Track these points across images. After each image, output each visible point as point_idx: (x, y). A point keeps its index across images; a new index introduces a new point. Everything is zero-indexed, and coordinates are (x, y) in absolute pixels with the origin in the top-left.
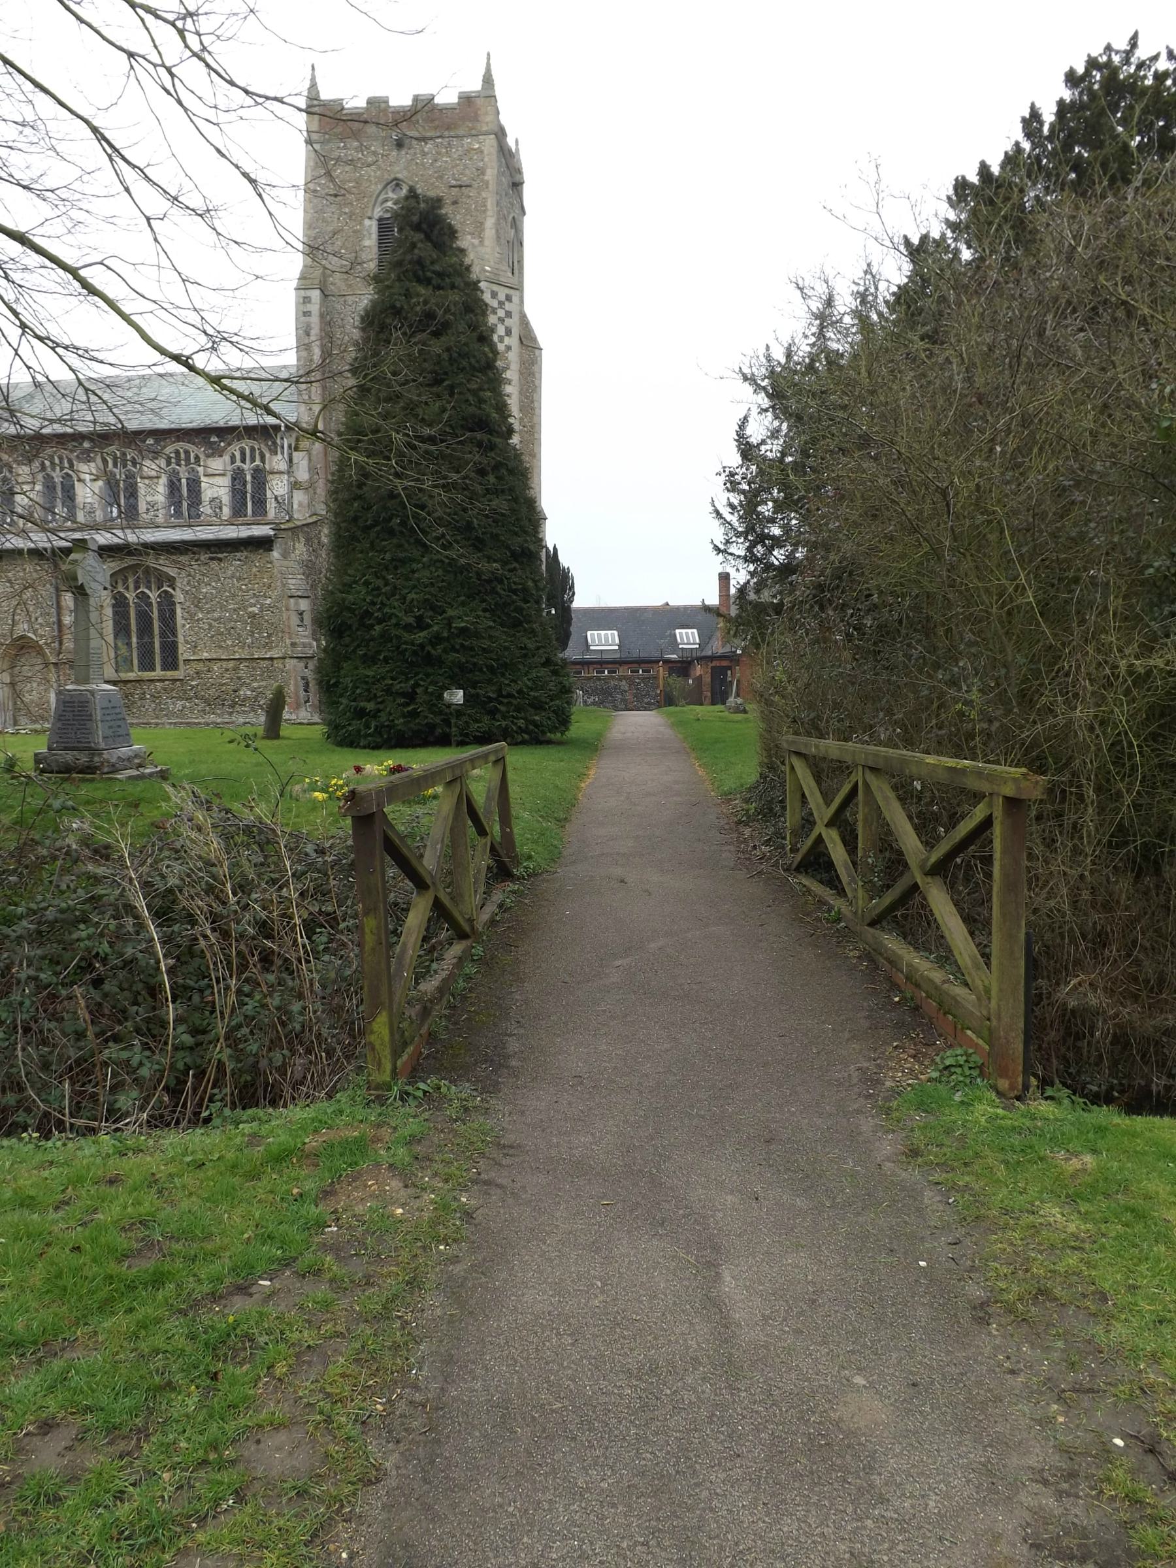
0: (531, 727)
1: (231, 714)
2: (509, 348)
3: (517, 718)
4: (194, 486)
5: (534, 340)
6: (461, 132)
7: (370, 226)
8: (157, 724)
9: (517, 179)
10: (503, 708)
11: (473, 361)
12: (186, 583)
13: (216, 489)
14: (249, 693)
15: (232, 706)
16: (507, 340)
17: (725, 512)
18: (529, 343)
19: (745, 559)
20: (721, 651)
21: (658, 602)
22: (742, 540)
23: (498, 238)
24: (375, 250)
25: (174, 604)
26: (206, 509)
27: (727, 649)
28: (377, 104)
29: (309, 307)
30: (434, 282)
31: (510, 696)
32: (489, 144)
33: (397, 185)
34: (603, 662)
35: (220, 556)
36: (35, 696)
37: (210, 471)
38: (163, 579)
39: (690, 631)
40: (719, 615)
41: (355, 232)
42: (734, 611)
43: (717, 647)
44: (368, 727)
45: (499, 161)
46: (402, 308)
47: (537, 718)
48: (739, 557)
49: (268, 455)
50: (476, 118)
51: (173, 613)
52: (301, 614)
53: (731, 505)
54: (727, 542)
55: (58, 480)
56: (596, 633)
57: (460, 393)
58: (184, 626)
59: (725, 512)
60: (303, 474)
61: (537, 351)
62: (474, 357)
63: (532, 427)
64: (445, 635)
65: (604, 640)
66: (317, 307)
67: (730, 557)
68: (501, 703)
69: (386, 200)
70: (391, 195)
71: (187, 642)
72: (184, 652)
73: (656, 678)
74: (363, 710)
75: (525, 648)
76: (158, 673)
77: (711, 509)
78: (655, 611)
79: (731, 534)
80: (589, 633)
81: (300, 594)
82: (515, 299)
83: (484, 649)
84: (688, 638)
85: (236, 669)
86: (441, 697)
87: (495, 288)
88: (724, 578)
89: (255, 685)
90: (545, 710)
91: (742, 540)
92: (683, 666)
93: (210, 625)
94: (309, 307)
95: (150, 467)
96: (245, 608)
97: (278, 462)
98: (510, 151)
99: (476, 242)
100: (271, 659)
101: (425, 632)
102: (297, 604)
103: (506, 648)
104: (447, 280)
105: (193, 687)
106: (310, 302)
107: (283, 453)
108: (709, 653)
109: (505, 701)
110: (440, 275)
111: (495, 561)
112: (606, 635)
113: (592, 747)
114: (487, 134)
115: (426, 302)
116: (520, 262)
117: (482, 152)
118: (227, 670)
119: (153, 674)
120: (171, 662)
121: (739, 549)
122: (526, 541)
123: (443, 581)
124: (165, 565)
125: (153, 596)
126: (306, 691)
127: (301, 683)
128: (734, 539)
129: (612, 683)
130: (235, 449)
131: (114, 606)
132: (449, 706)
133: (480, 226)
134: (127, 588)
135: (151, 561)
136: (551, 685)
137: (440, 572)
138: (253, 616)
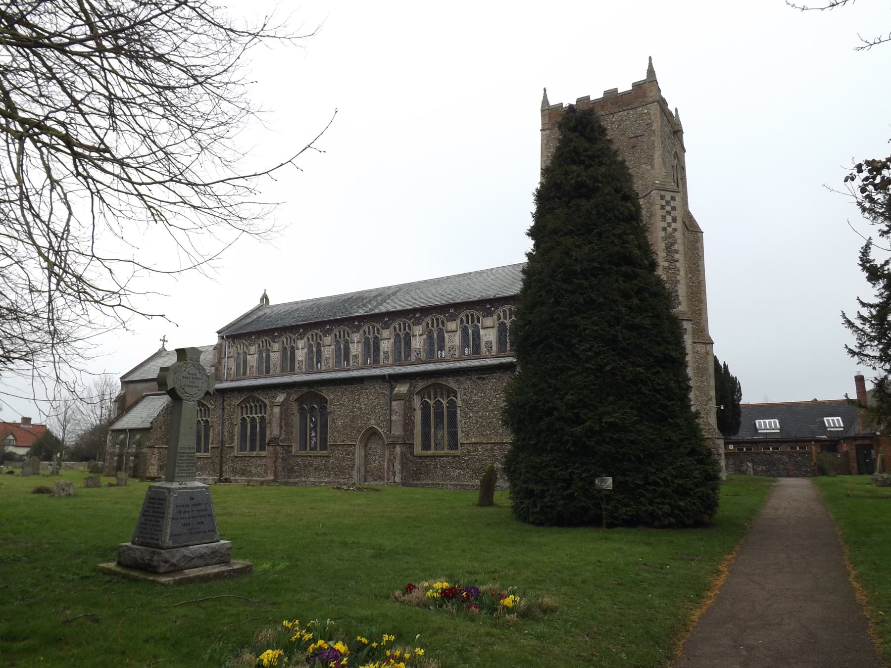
0: (677, 512)
2: (675, 230)
3: (663, 503)
4: (477, 336)
5: (697, 226)
6: (635, 106)
8: (443, 485)
9: (676, 128)
10: (649, 495)
11: (617, 213)
16: (673, 225)
17: (858, 323)
18: (693, 231)
19: (881, 359)
20: (862, 433)
21: (809, 399)
22: (876, 343)
23: (664, 163)
26: (483, 349)
27: (868, 431)
30: (587, 163)
31: (656, 484)
32: (655, 108)
34: (768, 441)
38: (452, 392)
39: (835, 418)
40: (861, 406)
42: (872, 402)
43: (858, 429)
44: (535, 506)
45: (661, 117)
46: (562, 183)
47: (682, 503)
48: (874, 357)
50: (644, 95)
53: (861, 317)
54: (862, 346)
55: (402, 336)
56: (762, 421)
57: (607, 237)
59: (858, 323)
61: (699, 234)
62: (618, 210)
63: (699, 283)
64: (597, 428)
65: (769, 425)
67: (865, 358)
68: (646, 490)
73: (810, 453)
74: (532, 491)
75: (670, 440)
77: (843, 320)
78: (806, 404)
79: (865, 339)
80: (757, 422)
82: (678, 198)
83: (632, 441)
84: (834, 423)
86: (592, 483)
87: (663, 193)
88: (860, 380)
90: (690, 496)
91: (876, 343)
92: (832, 443)
93: (477, 421)
95: (452, 325)
98: (671, 113)
99: (649, 167)
101: (581, 427)
103: (652, 441)
104: (597, 160)
108: (853, 434)
109: (651, 488)
110: (591, 158)
111: (639, 366)
112: (770, 423)
113: (738, 530)
114: (652, 102)
115: (578, 176)
116: (684, 178)
120: (453, 445)
121: (873, 350)
122: (668, 349)
123: (594, 385)
124: (452, 383)
125: (444, 402)
128: (868, 343)
129: (776, 457)
130: (500, 311)
131: (422, 409)
132: (600, 491)
133: (650, 159)
134: (430, 399)
135: (442, 381)
136: (696, 473)
137: (592, 377)
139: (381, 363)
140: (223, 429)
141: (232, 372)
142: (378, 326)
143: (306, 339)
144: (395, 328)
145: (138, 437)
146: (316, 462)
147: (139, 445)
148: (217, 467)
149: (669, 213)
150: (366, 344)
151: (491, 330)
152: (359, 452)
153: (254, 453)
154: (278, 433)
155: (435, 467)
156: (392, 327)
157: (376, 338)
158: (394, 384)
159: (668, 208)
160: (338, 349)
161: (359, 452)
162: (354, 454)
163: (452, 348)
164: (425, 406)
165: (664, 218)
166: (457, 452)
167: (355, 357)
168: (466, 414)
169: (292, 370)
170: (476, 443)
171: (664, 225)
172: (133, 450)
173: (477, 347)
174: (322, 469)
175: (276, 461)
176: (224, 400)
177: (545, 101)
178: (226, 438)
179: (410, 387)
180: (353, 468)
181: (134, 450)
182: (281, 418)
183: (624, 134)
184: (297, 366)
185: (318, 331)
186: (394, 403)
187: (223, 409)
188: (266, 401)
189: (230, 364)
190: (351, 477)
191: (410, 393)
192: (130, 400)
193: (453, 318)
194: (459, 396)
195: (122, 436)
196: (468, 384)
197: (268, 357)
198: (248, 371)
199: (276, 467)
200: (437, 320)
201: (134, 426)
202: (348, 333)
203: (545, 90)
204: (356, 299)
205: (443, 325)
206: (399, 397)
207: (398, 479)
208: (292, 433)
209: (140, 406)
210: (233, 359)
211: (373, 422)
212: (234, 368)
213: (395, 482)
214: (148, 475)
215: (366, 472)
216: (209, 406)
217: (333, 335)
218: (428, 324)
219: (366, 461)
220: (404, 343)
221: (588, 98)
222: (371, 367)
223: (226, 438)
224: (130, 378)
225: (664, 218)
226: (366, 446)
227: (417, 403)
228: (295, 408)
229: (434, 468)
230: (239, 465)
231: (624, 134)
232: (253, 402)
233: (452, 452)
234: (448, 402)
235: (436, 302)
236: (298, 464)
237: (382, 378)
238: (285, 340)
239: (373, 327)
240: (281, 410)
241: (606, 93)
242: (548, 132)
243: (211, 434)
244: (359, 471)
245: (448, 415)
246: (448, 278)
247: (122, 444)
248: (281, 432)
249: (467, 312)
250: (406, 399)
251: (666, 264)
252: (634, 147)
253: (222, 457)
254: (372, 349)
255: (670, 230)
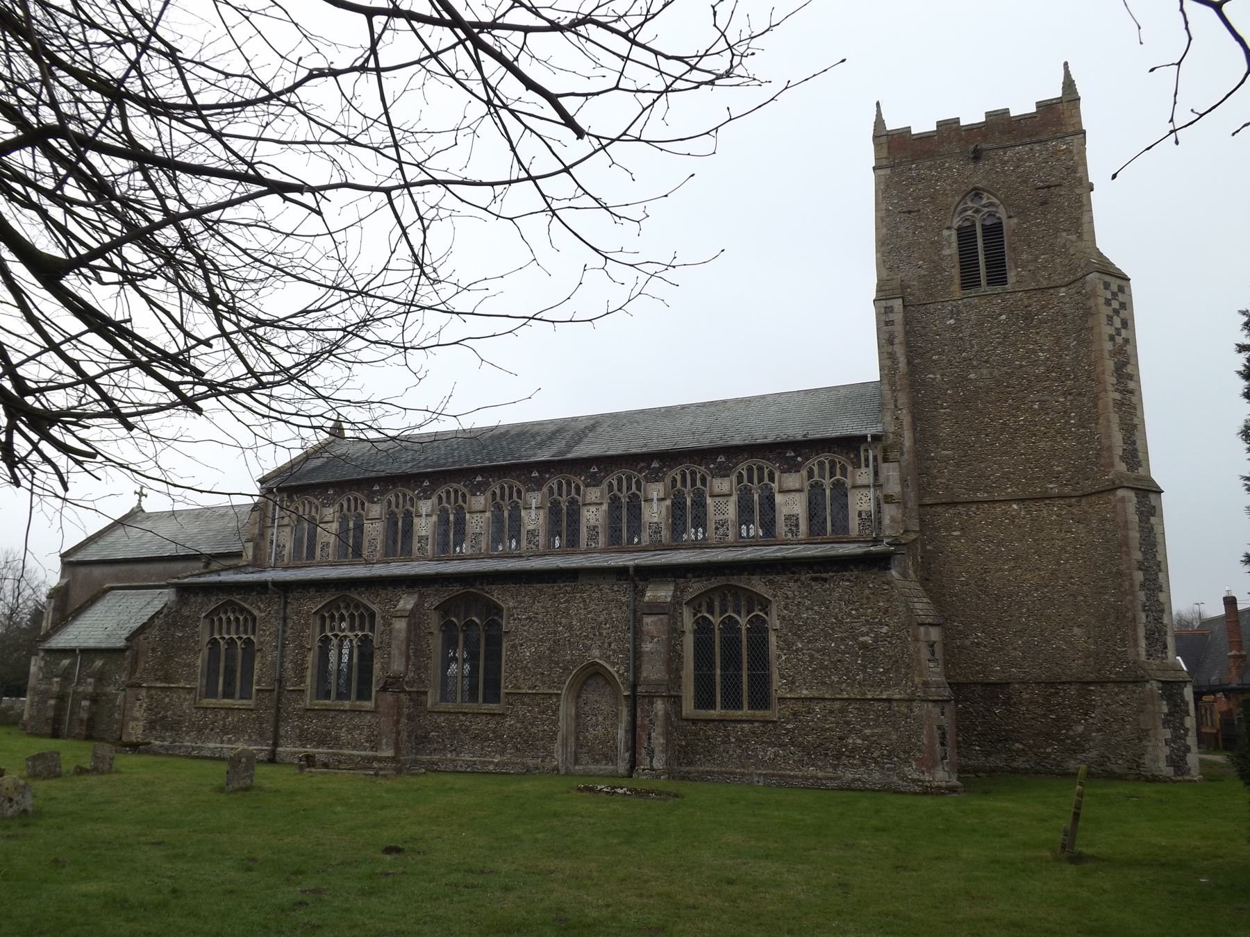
1: (835, 767)
7: (950, 236)
12: (783, 607)
13: (791, 505)
14: (859, 741)
15: (838, 757)
24: (956, 258)
25: (766, 630)
26: (781, 528)
28: (949, 128)
29: (891, 317)
33: (977, 194)
35: (824, 575)
36: (600, 731)
37: (785, 487)
41: (932, 243)
49: (709, 479)
51: (765, 642)
52: (932, 646)
58: (779, 657)
60: (894, 488)
66: (901, 315)
69: (965, 210)
70: (970, 204)
71: (782, 677)
72: (778, 685)
76: (745, 712)
81: (930, 620)
85: (843, 711)
87: (1107, 278)
89: (868, 732)
93: (811, 656)
94: (891, 317)
96: (855, 639)
97: (864, 476)
99: (1074, 237)
100: (889, 700)
102: (927, 633)
105: (788, 731)
106: (892, 311)
107: (867, 466)
117: (1071, 152)
118: (831, 712)
119: (740, 713)
120: (761, 698)
124: (758, 585)
125: (743, 621)
126: (943, 744)
127: (937, 734)
130: (813, 463)
131: (695, 632)
135: (741, 582)
138: (864, 646)
139: (583, 545)
140: (282, 656)
141: (286, 552)
142: (580, 480)
143: (435, 499)
144: (611, 485)
145: (99, 663)
146: (478, 725)
147: (101, 678)
148: (268, 727)
149: (1116, 312)
150: (554, 512)
151: (797, 496)
152: (566, 709)
153: (347, 704)
154: (402, 669)
155: (726, 742)
156: (605, 485)
157: (573, 502)
158: (641, 584)
159: (1115, 305)
160: (497, 520)
161: (566, 709)
162: (555, 712)
163: (722, 524)
164: (703, 628)
165: (1110, 318)
166: (772, 714)
167: (421, 538)
168: (789, 645)
169: (407, 554)
170: (811, 699)
171: (1112, 331)
172: (89, 687)
173: (769, 525)
174: (488, 739)
175: (398, 722)
176: (286, 603)
177: (879, 122)
178: (289, 673)
179: (675, 591)
180: (553, 738)
181: (90, 689)
182: (408, 640)
183: (1025, 182)
184: (416, 545)
185: (460, 486)
186: (648, 620)
187: (285, 619)
188: (375, 608)
189: (282, 536)
190: (550, 754)
191: (677, 602)
192: (76, 599)
193: (723, 472)
194: (774, 610)
195: (66, 662)
196: (791, 588)
197: (359, 528)
198: (318, 552)
199: (398, 733)
200: (693, 473)
201: (91, 644)
202: (519, 492)
203: (878, 104)
204: (518, 435)
205: (578, 493)
206: (656, 608)
207: (658, 764)
208: (426, 669)
209: (99, 609)
210: (288, 530)
211: (596, 652)
212: (289, 546)
213: (652, 769)
214: (125, 739)
215: (579, 745)
216: (256, 612)
217: (489, 494)
218: (674, 480)
219: (578, 725)
220: (625, 515)
221: (1006, 111)
222: (562, 553)
223: (289, 673)
224: (79, 557)
225: (1110, 318)
226: (579, 696)
227: (688, 620)
228: (434, 622)
229: (724, 742)
230: (314, 724)
231: (1025, 182)
232: (347, 607)
233: (759, 713)
234: (750, 621)
235: (689, 443)
236: (438, 728)
237: (620, 573)
238: (393, 500)
239: (569, 484)
240: (409, 625)
241: (940, 124)
242: (888, 171)
243: (257, 666)
244: (565, 745)
245: (750, 646)
246: (683, 407)
247: (66, 676)
248: (407, 665)
249: (750, 462)
250: (669, 611)
251: (1117, 396)
252: (1044, 203)
253: (278, 709)
254: (564, 521)
255: (1119, 340)
